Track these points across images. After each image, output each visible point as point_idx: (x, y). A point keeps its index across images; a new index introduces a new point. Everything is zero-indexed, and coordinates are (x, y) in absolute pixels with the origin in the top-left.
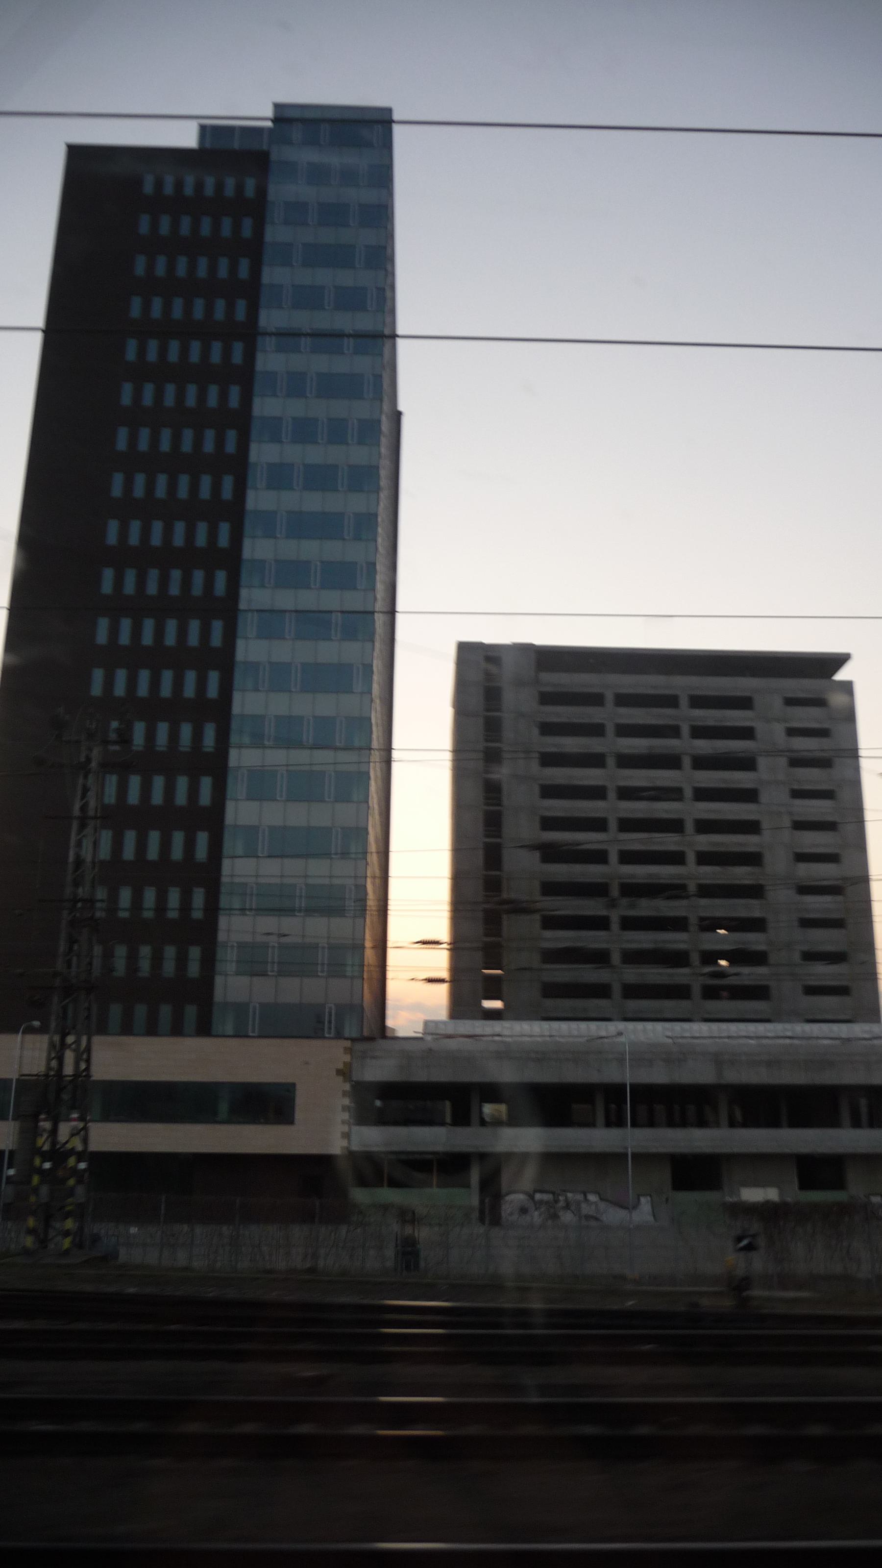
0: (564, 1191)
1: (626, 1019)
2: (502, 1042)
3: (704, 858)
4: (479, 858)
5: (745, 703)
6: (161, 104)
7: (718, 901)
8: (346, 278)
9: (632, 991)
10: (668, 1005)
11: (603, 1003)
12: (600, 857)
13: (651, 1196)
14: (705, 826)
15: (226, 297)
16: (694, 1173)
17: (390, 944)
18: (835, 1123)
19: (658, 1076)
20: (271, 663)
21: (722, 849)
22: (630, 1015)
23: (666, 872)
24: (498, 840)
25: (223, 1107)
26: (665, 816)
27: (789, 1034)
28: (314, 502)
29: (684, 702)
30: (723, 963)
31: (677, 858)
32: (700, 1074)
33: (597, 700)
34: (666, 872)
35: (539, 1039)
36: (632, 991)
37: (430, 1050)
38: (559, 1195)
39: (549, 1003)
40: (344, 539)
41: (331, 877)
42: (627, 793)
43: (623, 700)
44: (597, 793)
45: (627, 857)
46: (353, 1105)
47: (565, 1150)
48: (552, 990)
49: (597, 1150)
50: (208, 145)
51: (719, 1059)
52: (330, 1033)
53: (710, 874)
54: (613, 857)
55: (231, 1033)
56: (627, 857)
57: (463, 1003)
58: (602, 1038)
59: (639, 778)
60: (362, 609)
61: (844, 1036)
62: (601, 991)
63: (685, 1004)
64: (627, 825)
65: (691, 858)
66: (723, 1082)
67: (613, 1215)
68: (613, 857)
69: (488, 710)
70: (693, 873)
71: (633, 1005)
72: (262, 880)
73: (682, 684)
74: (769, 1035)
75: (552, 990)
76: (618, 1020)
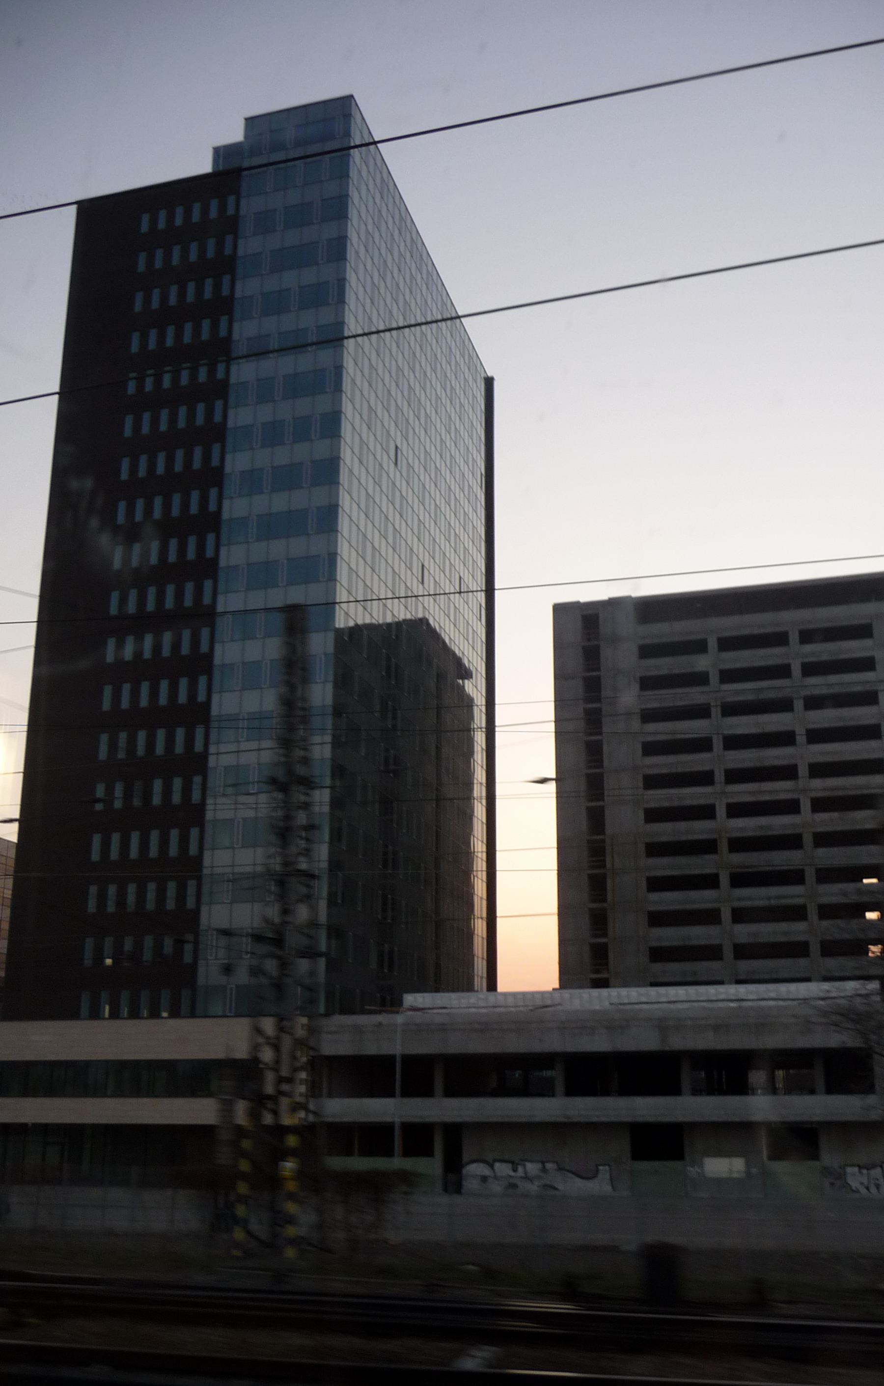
0: (522, 1160)
1: (739, 982)
2: (448, 1014)
3: (819, 805)
4: (583, 823)
5: (863, 631)
6: (170, 140)
7: (835, 850)
8: (309, 276)
9: (743, 952)
10: (784, 965)
11: (714, 965)
12: (706, 812)
13: (609, 1165)
14: (818, 770)
15: (219, 318)
16: (660, 1143)
17: (498, 914)
18: (674, 1090)
19: (600, 1043)
20: (243, 663)
21: (840, 793)
22: (742, 977)
23: (778, 824)
24: (601, 803)
25: (686, 1078)
26: (777, 763)
27: (773, 995)
28: (280, 502)
29: (794, 637)
30: (872, 916)
31: (791, 807)
32: (645, 1041)
33: (700, 647)
34: (778, 824)
35: (513, 1009)
36: (743, 952)
37: (444, 1024)
38: (518, 1164)
39: (658, 967)
40: (308, 534)
41: (254, 865)
42: (733, 742)
43: (727, 644)
44: (786, 739)
45: (736, 810)
46: (310, 1078)
47: (506, 1120)
48: (659, 954)
49: (538, 1119)
50: (221, 168)
51: (663, 1025)
52: (230, 1012)
53: (829, 821)
54: (721, 812)
55: (220, 1014)
56: (736, 810)
57: (570, 972)
58: (547, 1007)
59: (745, 725)
60: (499, 582)
61: (801, 997)
62: (712, 953)
63: (802, 963)
64: (818, 770)
65: (806, 806)
66: (667, 1048)
67: (573, 1186)
68: (721, 812)
69: (589, 670)
70: (808, 821)
71: (746, 966)
72: (237, 870)
73: (790, 619)
74: (751, 997)
75: (659, 954)
76: (730, 983)
